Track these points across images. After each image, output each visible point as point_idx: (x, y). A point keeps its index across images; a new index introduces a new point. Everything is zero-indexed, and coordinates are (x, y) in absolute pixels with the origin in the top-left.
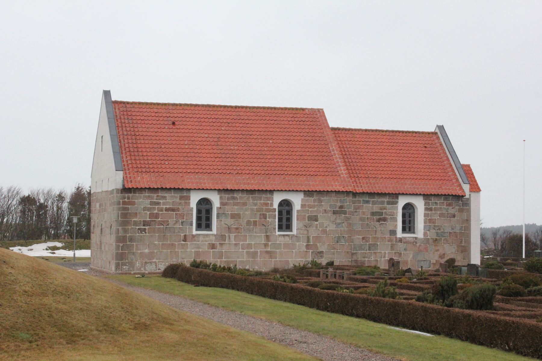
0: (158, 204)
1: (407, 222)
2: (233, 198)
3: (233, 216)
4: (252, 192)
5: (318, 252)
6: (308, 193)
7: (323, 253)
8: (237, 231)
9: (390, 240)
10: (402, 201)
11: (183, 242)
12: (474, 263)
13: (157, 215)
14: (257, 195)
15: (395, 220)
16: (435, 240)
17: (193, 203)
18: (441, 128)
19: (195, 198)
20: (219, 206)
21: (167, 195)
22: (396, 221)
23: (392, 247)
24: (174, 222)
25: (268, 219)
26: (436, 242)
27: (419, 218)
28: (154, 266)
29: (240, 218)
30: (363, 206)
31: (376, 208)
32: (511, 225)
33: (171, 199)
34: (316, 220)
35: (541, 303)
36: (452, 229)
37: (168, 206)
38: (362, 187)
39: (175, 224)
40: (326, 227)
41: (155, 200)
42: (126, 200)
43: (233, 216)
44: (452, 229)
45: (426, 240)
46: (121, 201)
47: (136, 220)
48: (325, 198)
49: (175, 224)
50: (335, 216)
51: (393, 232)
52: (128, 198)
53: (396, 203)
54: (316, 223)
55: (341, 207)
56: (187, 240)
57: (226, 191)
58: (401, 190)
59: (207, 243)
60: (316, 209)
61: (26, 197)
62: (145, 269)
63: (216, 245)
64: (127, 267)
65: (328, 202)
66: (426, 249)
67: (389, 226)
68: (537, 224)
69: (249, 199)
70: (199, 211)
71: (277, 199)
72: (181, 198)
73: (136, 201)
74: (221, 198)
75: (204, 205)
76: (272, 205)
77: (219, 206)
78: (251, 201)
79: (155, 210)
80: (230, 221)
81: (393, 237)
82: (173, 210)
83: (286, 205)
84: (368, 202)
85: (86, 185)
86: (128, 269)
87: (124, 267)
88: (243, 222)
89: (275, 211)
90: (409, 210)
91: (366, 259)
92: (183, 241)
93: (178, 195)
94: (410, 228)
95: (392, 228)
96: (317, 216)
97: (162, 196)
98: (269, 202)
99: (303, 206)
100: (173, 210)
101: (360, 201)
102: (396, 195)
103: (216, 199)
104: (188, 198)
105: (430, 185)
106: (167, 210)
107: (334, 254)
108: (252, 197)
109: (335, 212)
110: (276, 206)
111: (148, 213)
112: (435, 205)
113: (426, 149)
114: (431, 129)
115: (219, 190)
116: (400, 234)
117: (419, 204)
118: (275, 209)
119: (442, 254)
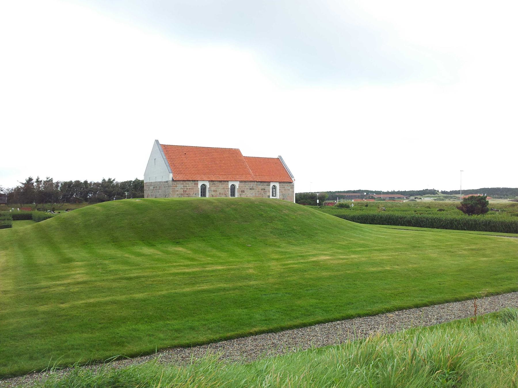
0: (186, 186)
1: (203, 192)
2: (214, 184)
3: (214, 191)
4: (221, 181)
6: (241, 182)
10: (272, 184)
13: (186, 191)
14: (223, 183)
15: (269, 192)
17: (199, 187)
18: (280, 157)
19: (200, 184)
20: (238, 188)
22: (270, 192)
27: (277, 189)
31: (263, 187)
32: (502, 188)
33: (191, 185)
34: (244, 192)
39: (193, 194)
43: (214, 191)
49: (193, 194)
51: (269, 196)
53: (270, 185)
54: (244, 193)
55: (253, 187)
57: (212, 181)
61: (117, 184)
68: (99, 182)
70: (201, 189)
71: (230, 184)
72: (195, 184)
74: (210, 184)
75: (204, 187)
76: (228, 186)
77: (238, 188)
80: (213, 193)
82: (192, 189)
83: (233, 187)
84: (260, 185)
85: (141, 178)
90: (274, 187)
94: (233, 194)
97: (188, 183)
99: (239, 187)
100: (192, 189)
102: (270, 182)
103: (207, 184)
104: (197, 184)
105: (207, 152)
106: (189, 189)
108: (221, 184)
109: (250, 189)
110: (230, 187)
111: (182, 190)
113: (276, 165)
114: (276, 156)
115: (209, 181)
116: (271, 197)
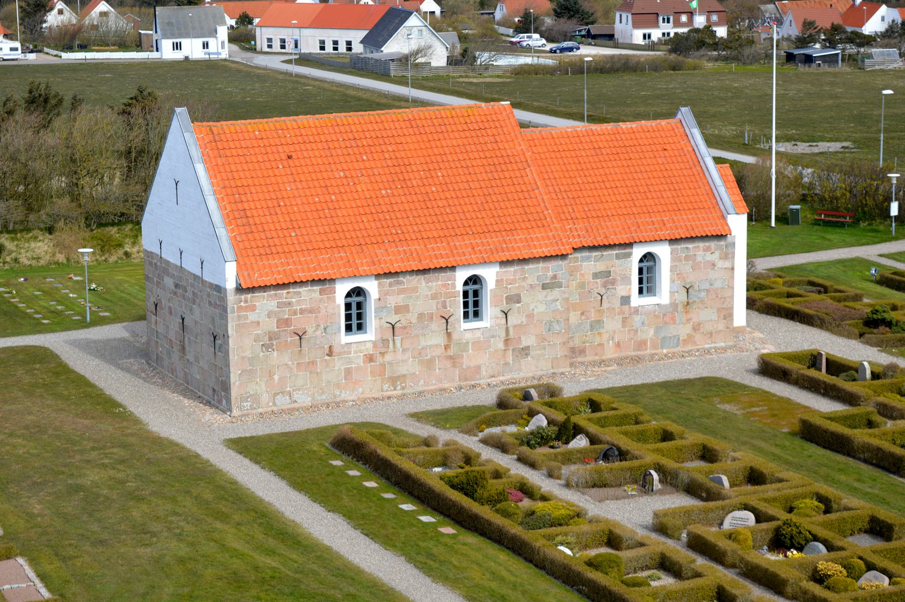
5: (522, 349)
7: (529, 350)
8: (405, 331)
9: (622, 312)
10: (638, 252)
11: (327, 358)
12: (307, 51)
16: (686, 304)
17: (340, 299)
19: (342, 288)
21: (303, 290)
23: (624, 320)
24: (314, 329)
25: (449, 308)
26: (688, 307)
28: (287, 397)
29: (408, 311)
30: (581, 265)
31: (601, 267)
33: (308, 295)
35: (903, 418)
36: (711, 285)
37: (303, 307)
38: (580, 237)
40: (533, 310)
41: (284, 300)
42: (242, 304)
44: (711, 285)
45: (674, 305)
46: (236, 306)
47: (258, 332)
48: (531, 266)
50: (545, 292)
52: (246, 301)
53: (629, 255)
54: (518, 305)
55: (555, 277)
56: (334, 354)
58: (636, 236)
59: (362, 354)
60: (517, 285)
62: (274, 404)
63: (375, 356)
64: (249, 404)
65: (535, 271)
66: (673, 320)
67: (621, 291)
69: (419, 282)
71: (462, 275)
73: (257, 304)
76: (454, 286)
78: (424, 284)
79: (285, 314)
81: (625, 308)
86: (250, 406)
87: (245, 404)
88: (413, 317)
89: (459, 296)
91: (588, 344)
92: (328, 355)
93: (317, 288)
95: (624, 294)
96: (519, 296)
98: (449, 282)
99: (498, 282)
100: (311, 311)
101: (577, 258)
103: (371, 286)
107: (545, 349)
109: (544, 287)
110: (460, 288)
112: (686, 251)
117: (663, 251)
118: (459, 291)
119: (696, 324)
